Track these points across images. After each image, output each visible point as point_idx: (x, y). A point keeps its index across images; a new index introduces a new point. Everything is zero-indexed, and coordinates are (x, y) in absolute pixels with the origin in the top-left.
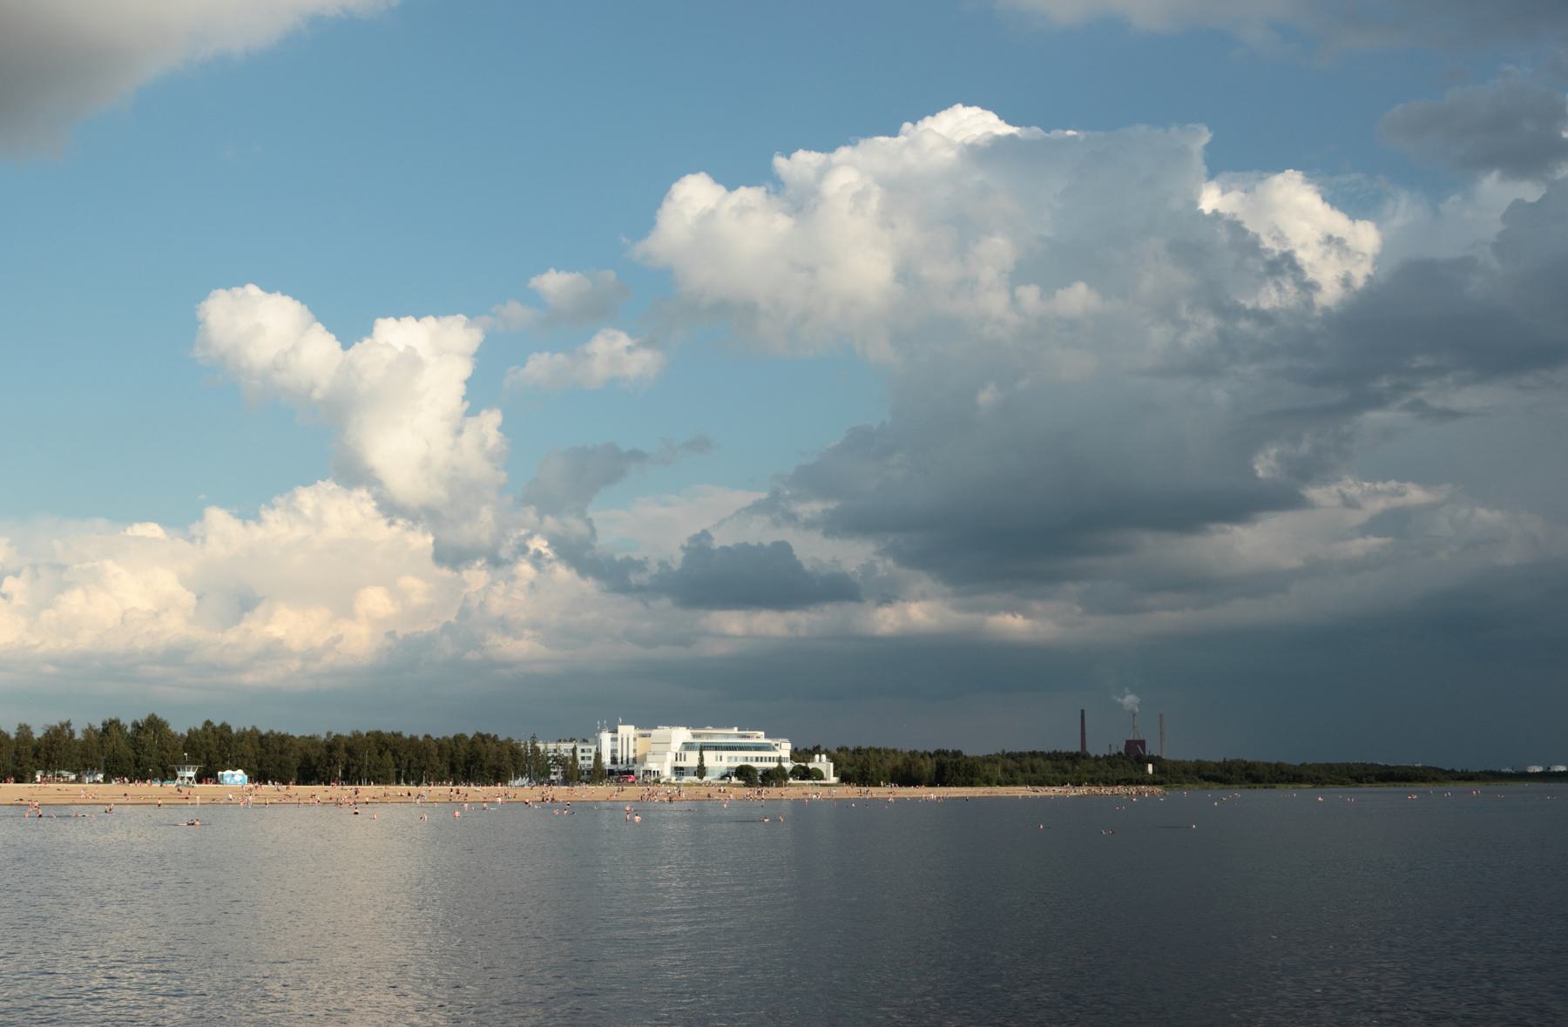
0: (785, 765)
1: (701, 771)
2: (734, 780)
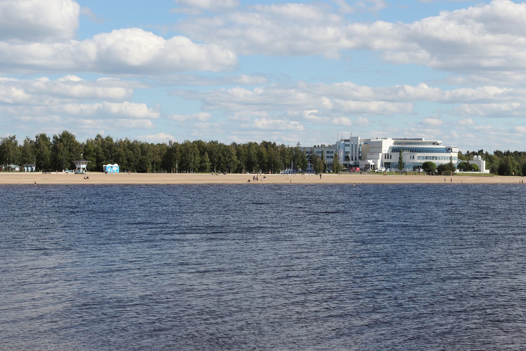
2: (421, 170)
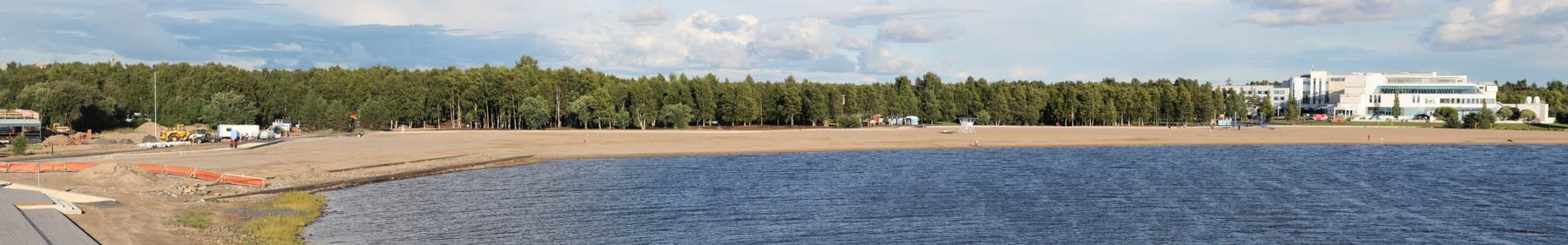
0: (1489, 106)
1: (1396, 111)
2: (1432, 119)
